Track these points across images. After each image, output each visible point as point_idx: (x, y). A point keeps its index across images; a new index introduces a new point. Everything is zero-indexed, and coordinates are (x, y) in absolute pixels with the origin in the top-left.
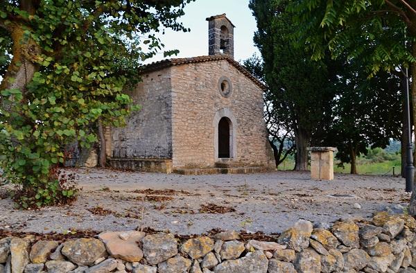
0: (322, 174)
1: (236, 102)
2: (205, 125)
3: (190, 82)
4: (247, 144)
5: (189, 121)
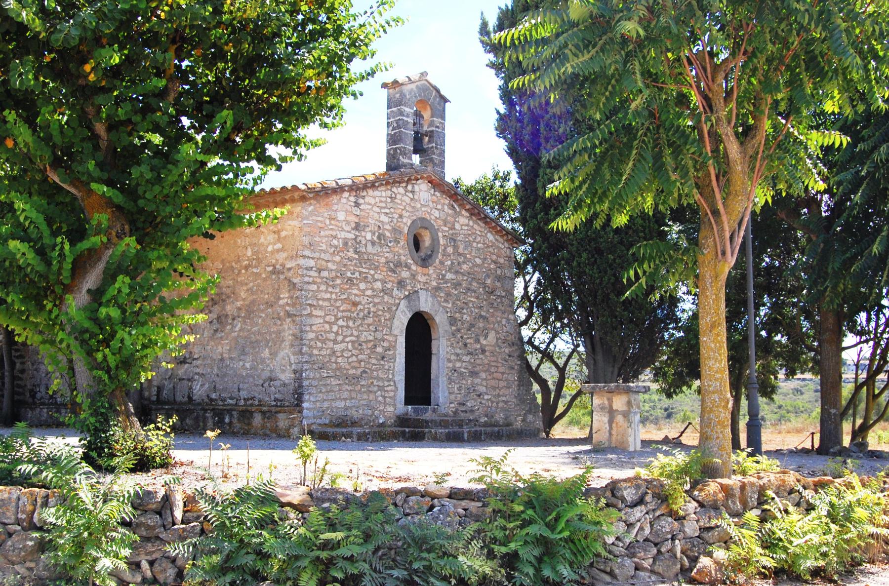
0: (614, 438)
1: (449, 276)
2: (376, 330)
3: (344, 235)
4: (474, 374)
5: (341, 322)
